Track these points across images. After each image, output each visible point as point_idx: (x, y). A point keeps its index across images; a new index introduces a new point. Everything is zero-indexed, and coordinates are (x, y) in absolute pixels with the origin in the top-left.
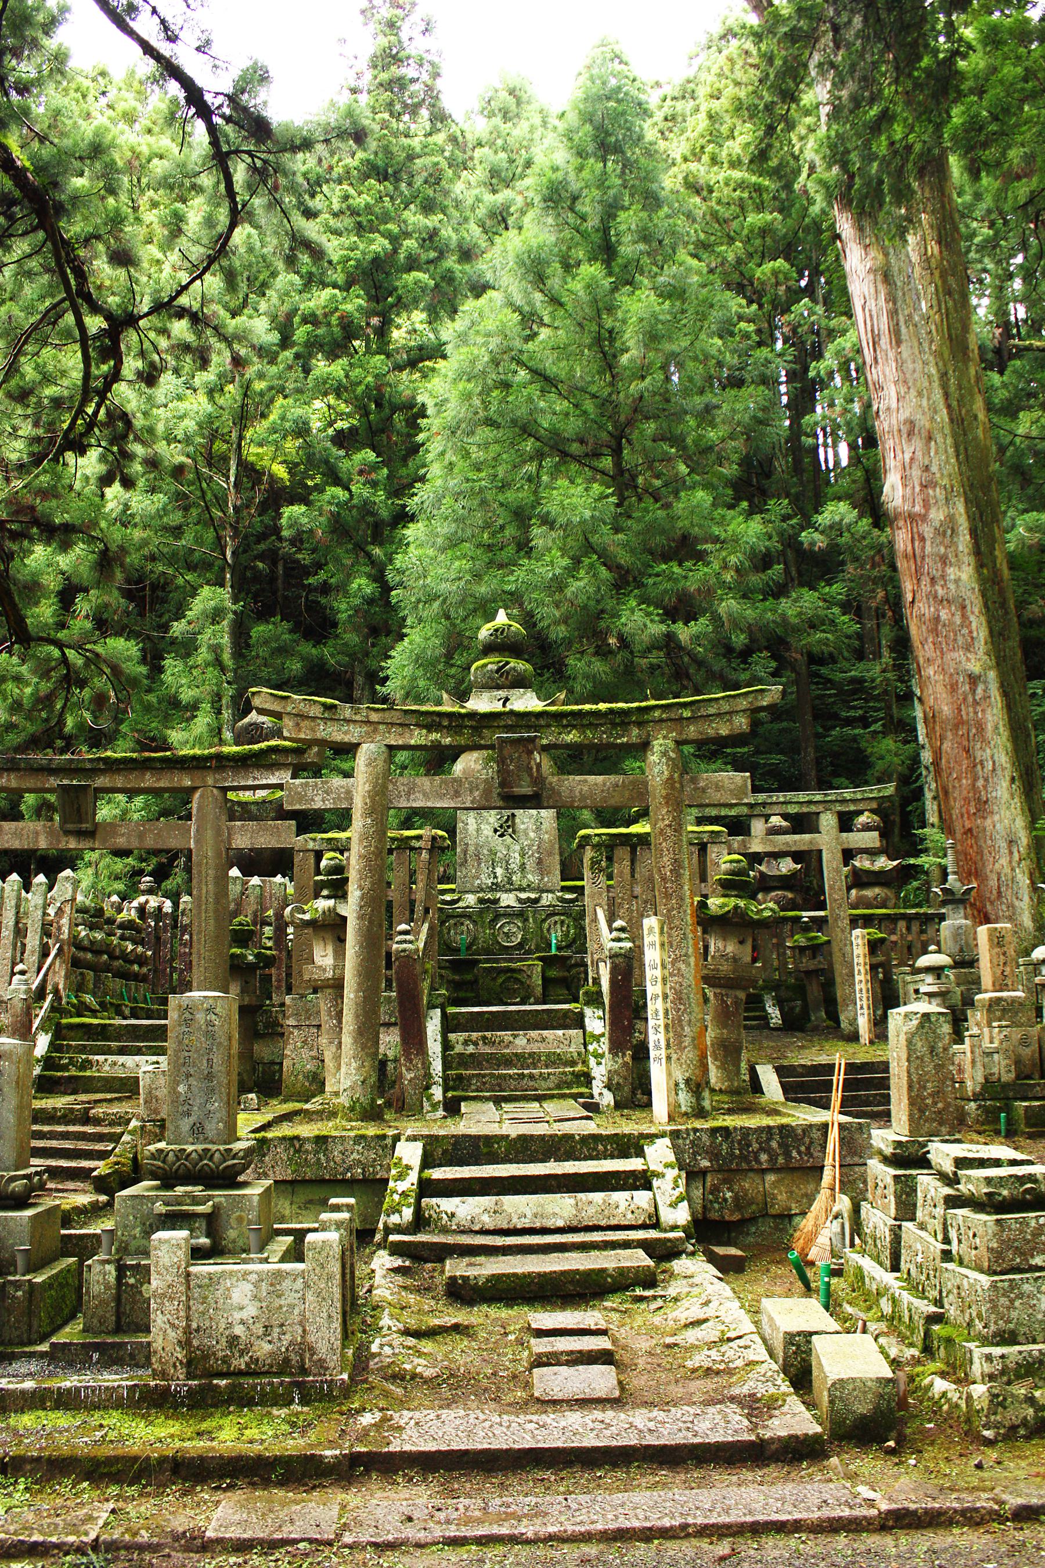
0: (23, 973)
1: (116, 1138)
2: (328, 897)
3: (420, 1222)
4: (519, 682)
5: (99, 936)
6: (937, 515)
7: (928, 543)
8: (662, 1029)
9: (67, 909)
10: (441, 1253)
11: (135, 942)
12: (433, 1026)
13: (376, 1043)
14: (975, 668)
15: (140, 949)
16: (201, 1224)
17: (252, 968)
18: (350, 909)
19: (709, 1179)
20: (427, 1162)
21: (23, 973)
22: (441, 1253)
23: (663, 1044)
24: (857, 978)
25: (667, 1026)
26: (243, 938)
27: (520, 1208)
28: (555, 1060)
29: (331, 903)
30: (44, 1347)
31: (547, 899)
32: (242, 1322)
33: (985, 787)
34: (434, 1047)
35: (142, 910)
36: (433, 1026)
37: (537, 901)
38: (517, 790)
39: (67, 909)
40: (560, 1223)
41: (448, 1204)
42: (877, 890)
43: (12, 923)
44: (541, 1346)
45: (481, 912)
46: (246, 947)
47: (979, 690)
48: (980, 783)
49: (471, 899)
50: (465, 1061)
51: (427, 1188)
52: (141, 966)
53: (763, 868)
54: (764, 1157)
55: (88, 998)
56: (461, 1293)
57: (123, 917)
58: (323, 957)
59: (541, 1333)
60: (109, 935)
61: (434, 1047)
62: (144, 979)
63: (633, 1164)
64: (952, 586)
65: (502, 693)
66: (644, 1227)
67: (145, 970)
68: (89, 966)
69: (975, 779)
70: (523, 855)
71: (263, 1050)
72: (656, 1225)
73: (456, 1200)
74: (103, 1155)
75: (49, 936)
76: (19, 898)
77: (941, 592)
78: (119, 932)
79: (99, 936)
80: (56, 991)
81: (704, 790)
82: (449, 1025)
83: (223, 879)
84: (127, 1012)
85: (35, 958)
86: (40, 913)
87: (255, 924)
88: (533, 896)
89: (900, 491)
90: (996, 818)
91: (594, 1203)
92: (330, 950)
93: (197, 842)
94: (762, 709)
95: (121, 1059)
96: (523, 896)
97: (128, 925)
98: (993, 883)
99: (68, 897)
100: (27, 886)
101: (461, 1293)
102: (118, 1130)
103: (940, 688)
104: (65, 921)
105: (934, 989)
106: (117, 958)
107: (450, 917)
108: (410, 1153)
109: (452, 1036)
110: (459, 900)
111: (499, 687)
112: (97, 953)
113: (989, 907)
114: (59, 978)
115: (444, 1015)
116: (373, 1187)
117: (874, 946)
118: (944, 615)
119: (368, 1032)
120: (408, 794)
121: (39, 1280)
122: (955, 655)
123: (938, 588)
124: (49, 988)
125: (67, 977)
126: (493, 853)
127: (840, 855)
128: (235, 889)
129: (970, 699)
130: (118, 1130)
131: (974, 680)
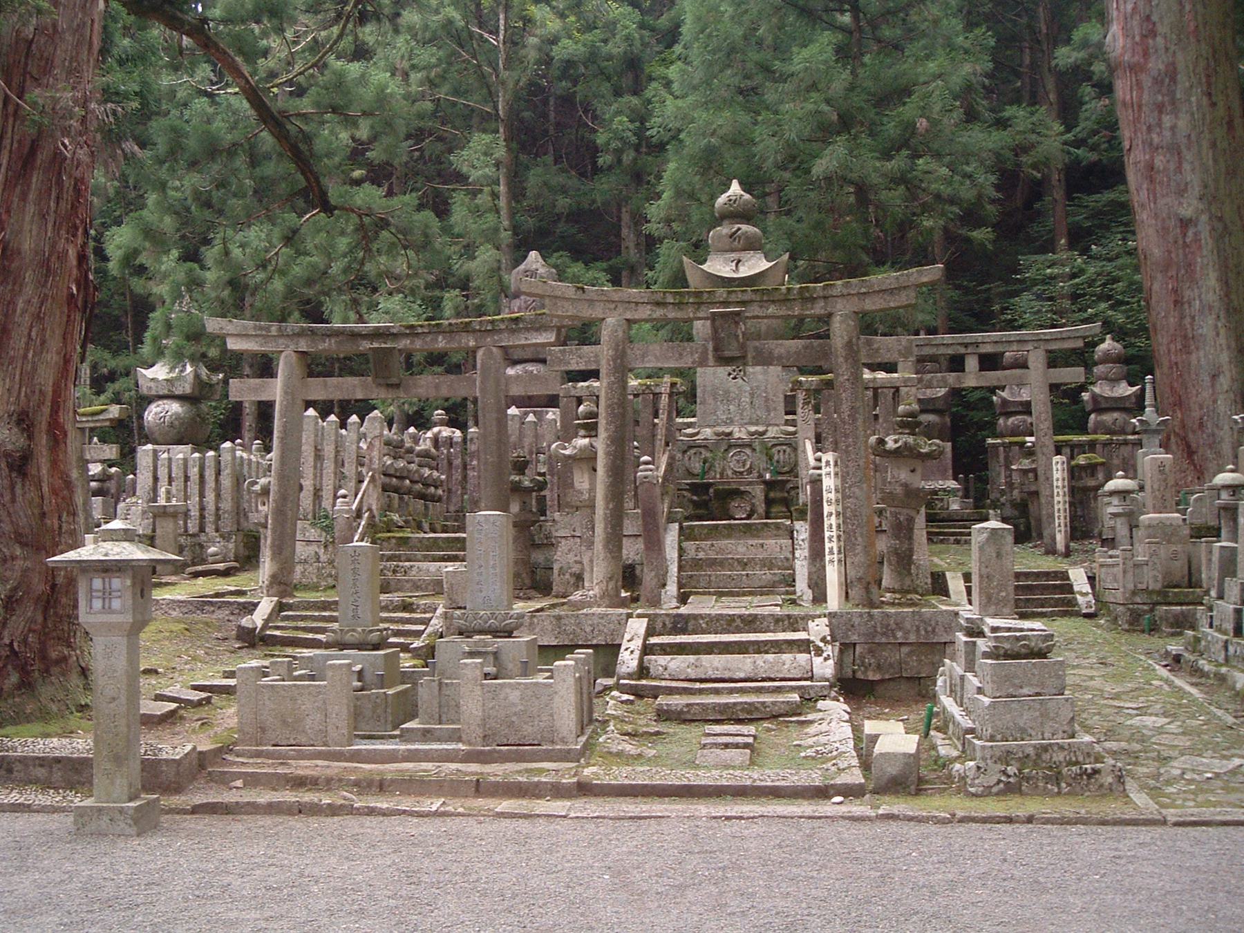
0: (344, 497)
1: (426, 622)
2: (585, 437)
3: (643, 672)
4: (751, 245)
5: (401, 464)
6: (1156, 65)
7: (1146, 92)
8: (835, 539)
9: (377, 443)
10: (655, 693)
11: (431, 468)
12: (671, 537)
13: (620, 548)
14: (1187, 211)
15: (435, 474)
16: (491, 658)
17: (529, 491)
18: (601, 444)
19: (858, 648)
20: (650, 632)
21: (344, 497)
22: (655, 693)
23: (835, 550)
24: (1056, 499)
25: (839, 537)
26: (521, 467)
27: (714, 664)
28: (769, 564)
29: (586, 441)
30: (397, 732)
31: (772, 432)
32: (515, 714)
33: (1192, 324)
34: (672, 554)
35: (436, 441)
36: (671, 537)
37: (764, 433)
38: (727, 354)
39: (377, 443)
40: (742, 675)
41: (662, 660)
42: (1116, 415)
43: (332, 456)
44: (710, 740)
45: (717, 443)
46: (524, 474)
47: (1190, 234)
48: (1187, 320)
49: (707, 432)
50: (697, 564)
51: (647, 650)
52: (436, 487)
53: (1004, 394)
54: (899, 634)
55: (396, 517)
56: (664, 715)
57: (421, 447)
58: (581, 481)
59: (709, 735)
60: (409, 463)
61: (672, 554)
62: (439, 500)
63: (801, 635)
64: (1167, 134)
65: (734, 255)
66: (806, 679)
67: (440, 492)
68: (396, 490)
69: (1182, 318)
70: (752, 395)
71: (538, 557)
72: (811, 679)
73: (668, 657)
74: (418, 634)
75: (362, 465)
76: (338, 435)
77: (1156, 139)
78: (417, 460)
79: (401, 464)
80: (370, 509)
81: (877, 350)
82: (685, 535)
83: (502, 419)
84: (426, 526)
85: (352, 484)
86: (354, 447)
87: (531, 453)
88: (761, 429)
89: (1120, 42)
90: (1201, 353)
91: (764, 662)
92: (586, 476)
93: (482, 390)
94: (924, 284)
95: (424, 565)
96: (753, 429)
97: (425, 454)
98: (1196, 414)
99: (377, 432)
100: (343, 425)
101: (664, 715)
102: (428, 615)
103: (1151, 231)
104: (375, 453)
105: (1120, 510)
106: (417, 482)
107: (691, 447)
108: (637, 626)
109: (685, 544)
110: (697, 434)
111: (733, 251)
112: (401, 478)
113: (1191, 436)
114: (374, 502)
115: (681, 528)
116: (610, 650)
117: (1074, 472)
118: (1159, 161)
119: (615, 539)
120: (643, 356)
121: (390, 692)
122: (1169, 200)
123: (1154, 136)
124: (365, 508)
125: (378, 499)
126: (727, 392)
127: (1047, 389)
128: (513, 427)
129: (1181, 242)
130: (428, 615)
131: (1185, 223)
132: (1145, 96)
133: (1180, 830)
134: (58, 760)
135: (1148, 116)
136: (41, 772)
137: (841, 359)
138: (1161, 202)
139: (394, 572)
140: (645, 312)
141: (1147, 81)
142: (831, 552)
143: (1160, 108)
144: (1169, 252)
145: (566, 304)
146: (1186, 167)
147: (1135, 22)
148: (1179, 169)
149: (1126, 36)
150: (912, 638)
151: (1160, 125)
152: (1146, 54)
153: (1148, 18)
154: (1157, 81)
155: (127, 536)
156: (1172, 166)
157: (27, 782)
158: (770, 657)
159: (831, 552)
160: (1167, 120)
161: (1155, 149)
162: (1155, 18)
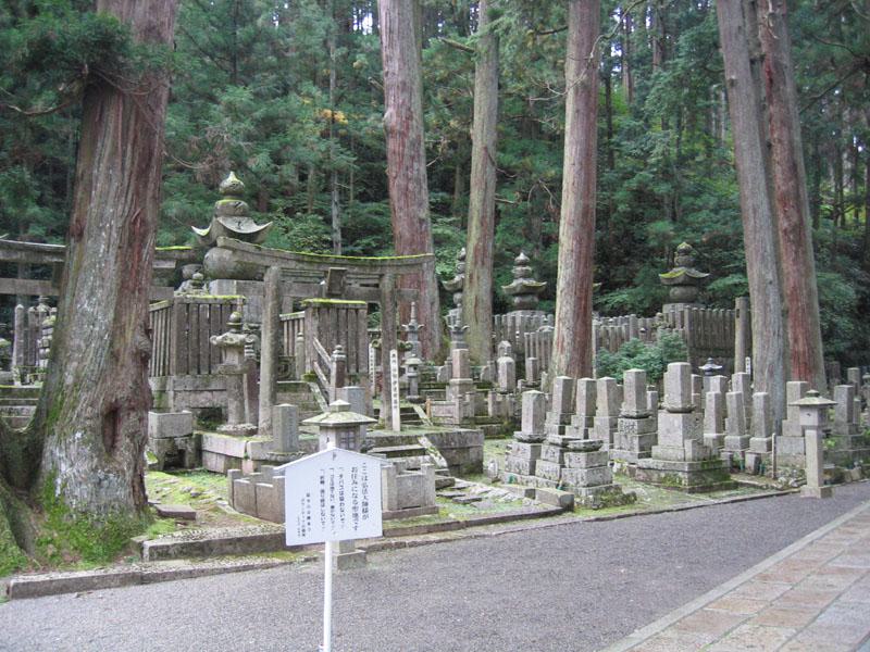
6: (412, 135)
38: (333, 292)
64: (415, 172)
96: (253, 325)
118: (411, 186)
131: (422, 221)
132: (406, 150)
133: (680, 512)
134: (239, 540)
135: (407, 162)
136: (229, 548)
137: (388, 300)
138: (411, 209)
139: (10, 413)
140: (293, 265)
141: (407, 143)
142: (396, 402)
143: (413, 158)
144: (413, 235)
145: (249, 255)
146: (423, 191)
147: (404, 110)
148: (420, 192)
149: (398, 116)
150: (458, 446)
151: (412, 167)
152: (408, 128)
153: (409, 109)
154: (413, 144)
155: (343, 409)
156: (417, 190)
157: (222, 554)
158: (413, 458)
159: (396, 402)
160: (416, 165)
161: (409, 179)
162: (412, 109)
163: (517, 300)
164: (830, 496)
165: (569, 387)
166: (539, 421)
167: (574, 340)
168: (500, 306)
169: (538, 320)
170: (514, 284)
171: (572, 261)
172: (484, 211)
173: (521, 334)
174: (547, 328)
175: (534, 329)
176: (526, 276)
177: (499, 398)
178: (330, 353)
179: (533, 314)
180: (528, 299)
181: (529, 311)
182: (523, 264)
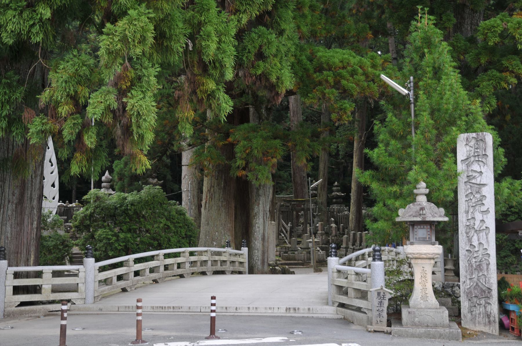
131: (304, 177)
163: (334, 200)
164: (165, 266)
165: (354, 235)
166: (347, 244)
167: (356, 219)
168: (329, 202)
169: (343, 209)
170: (333, 194)
171: (355, 194)
172: (324, 171)
173: (336, 214)
174: (346, 213)
175: (342, 212)
176: (338, 191)
177: (333, 238)
178: (287, 224)
179: (340, 207)
180: (338, 200)
181: (339, 205)
182: (337, 186)
